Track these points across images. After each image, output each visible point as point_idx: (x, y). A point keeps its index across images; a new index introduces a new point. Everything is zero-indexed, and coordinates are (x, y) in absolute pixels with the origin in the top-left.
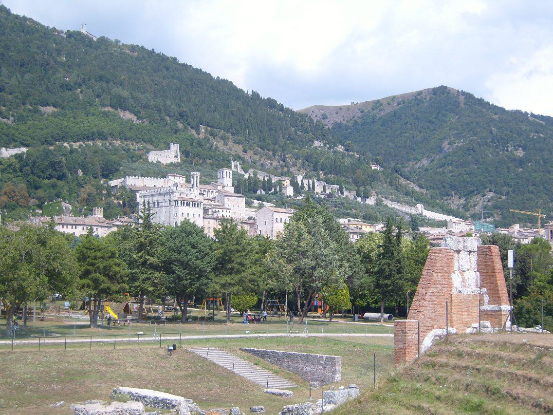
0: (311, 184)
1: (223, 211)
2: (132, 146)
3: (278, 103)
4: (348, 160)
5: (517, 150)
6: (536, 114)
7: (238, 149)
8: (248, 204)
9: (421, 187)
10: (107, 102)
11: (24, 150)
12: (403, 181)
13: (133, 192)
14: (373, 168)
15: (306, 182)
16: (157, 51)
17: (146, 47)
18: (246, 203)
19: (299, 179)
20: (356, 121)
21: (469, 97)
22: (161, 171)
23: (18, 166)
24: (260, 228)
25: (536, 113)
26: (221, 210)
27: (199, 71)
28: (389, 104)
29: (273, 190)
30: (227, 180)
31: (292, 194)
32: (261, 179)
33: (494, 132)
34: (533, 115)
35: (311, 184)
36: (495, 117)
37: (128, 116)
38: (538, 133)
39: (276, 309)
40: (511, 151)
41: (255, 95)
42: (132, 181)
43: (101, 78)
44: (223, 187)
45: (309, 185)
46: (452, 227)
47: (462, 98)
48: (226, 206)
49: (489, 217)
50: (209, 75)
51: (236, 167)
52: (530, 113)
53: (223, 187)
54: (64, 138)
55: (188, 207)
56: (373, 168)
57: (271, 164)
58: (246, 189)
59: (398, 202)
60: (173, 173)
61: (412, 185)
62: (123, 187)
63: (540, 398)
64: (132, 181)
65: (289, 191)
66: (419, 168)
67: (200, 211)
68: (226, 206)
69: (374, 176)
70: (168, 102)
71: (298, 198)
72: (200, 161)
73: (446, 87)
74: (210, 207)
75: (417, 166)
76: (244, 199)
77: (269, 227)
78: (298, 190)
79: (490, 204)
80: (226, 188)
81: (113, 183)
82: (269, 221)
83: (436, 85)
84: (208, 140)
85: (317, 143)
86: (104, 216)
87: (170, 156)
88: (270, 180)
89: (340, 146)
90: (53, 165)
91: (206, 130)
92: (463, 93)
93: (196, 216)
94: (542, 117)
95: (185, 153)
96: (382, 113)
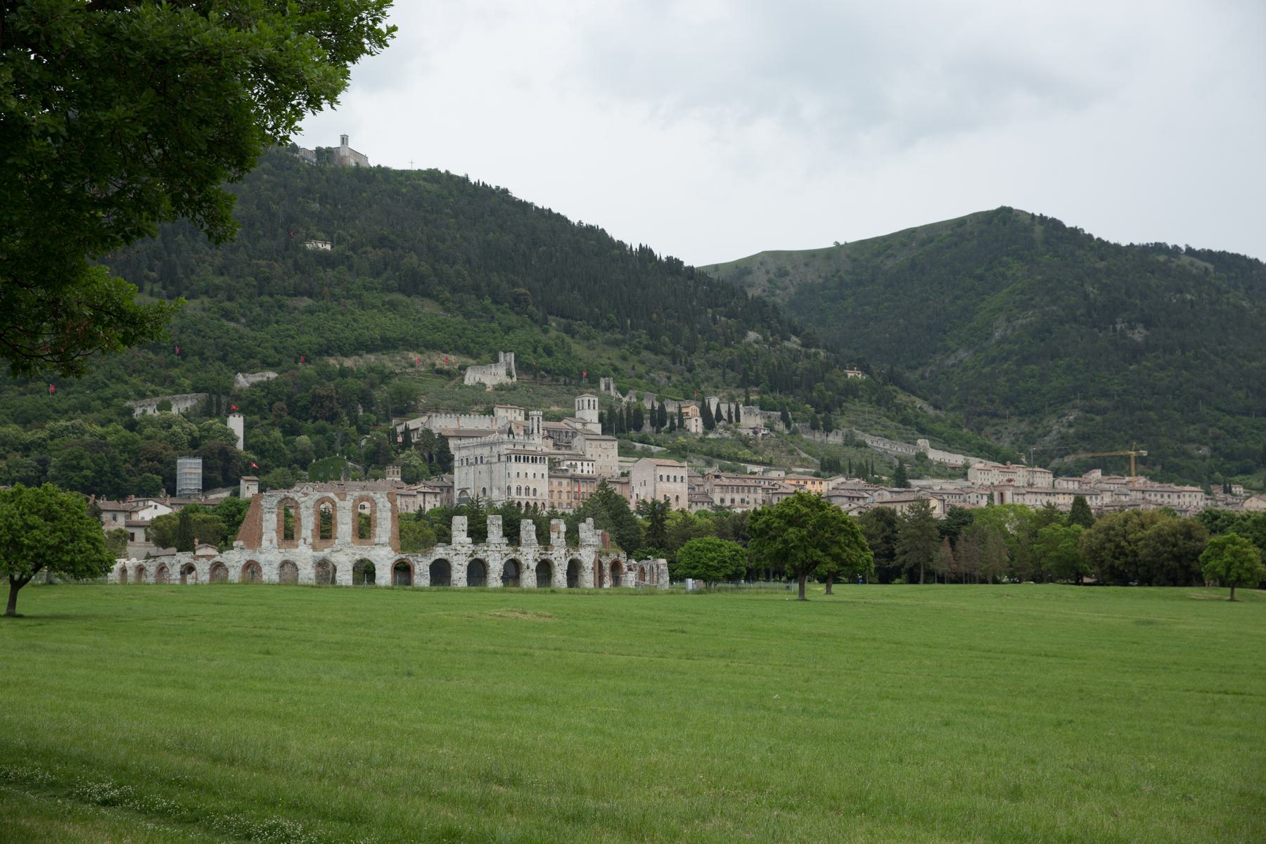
0: (733, 410)
1: (560, 484)
2: (440, 360)
3: (686, 264)
4: (803, 364)
5: (1132, 328)
6: (1197, 249)
7: (611, 356)
8: (624, 451)
9: (936, 407)
10: (393, 283)
11: (272, 375)
12: (902, 398)
13: (444, 439)
14: (850, 375)
15: (724, 408)
16: (473, 180)
17: (453, 172)
18: (620, 447)
19: (713, 403)
20: (840, 278)
21: (1054, 225)
22: (484, 403)
23: (265, 402)
24: (636, 491)
25: (1197, 247)
26: (579, 463)
27: (547, 215)
28: (904, 245)
29: (668, 425)
30: (589, 412)
31: (700, 430)
32: (648, 406)
33: (1092, 296)
34: (1190, 251)
35: (733, 410)
36: (1101, 265)
37: (428, 308)
38: (1182, 292)
39: (133, 316)
40: (1122, 330)
41: (646, 253)
42: (442, 423)
43: (382, 242)
44: (584, 424)
45: (729, 413)
46: (976, 478)
47: (1039, 229)
48: (588, 456)
49: (1068, 454)
50: (561, 219)
51: (608, 388)
52: (1184, 249)
53: (584, 424)
54: (326, 351)
55: (526, 465)
56: (850, 375)
57: (669, 378)
58: (618, 425)
59: (886, 437)
60: (504, 403)
61: (919, 403)
62: (428, 432)
63: (695, 592)
64: (442, 423)
65: (695, 425)
66: (953, 365)
67: (543, 468)
68: (588, 456)
69: (851, 390)
70: (495, 278)
71: (711, 436)
72: (549, 378)
73: (1010, 210)
74: (561, 458)
75: (950, 362)
76: (616, 444)
77: (651, 489)
78: (710, 422)
79: (1072, 431)
80: (589, 427)
81: (413, 424)
82: (650, 480)
83: (993, 206)
84: (563, 341)
85: (752, 336)
86: (403, 479)
87: (493, 376)
88: (662, 408)
89: (794, 338)
90: (317, 400)
91: (559, 324)
92: (1042, 219)
93: (539, 476)
94: (1208, 255)
95: (523, 367)
96: (890, 263)
